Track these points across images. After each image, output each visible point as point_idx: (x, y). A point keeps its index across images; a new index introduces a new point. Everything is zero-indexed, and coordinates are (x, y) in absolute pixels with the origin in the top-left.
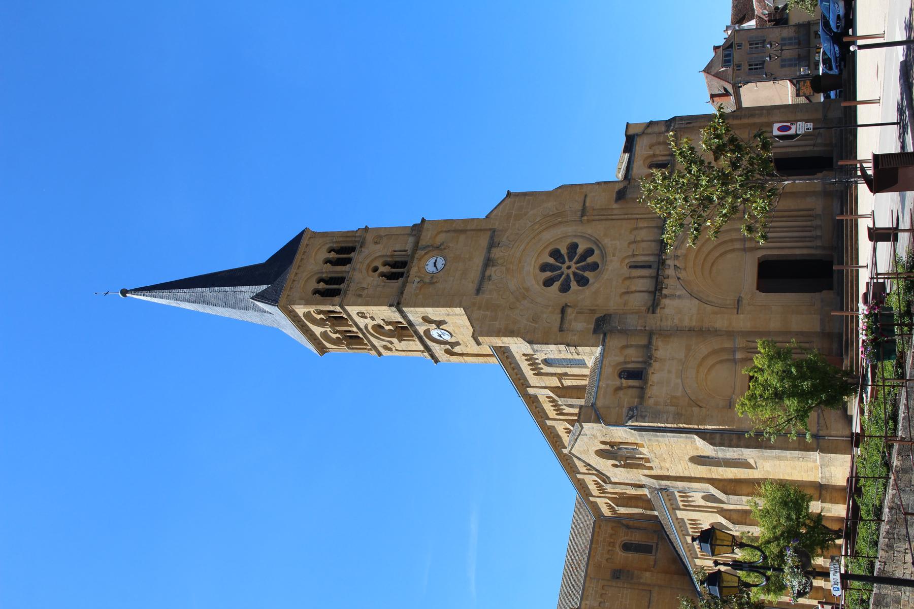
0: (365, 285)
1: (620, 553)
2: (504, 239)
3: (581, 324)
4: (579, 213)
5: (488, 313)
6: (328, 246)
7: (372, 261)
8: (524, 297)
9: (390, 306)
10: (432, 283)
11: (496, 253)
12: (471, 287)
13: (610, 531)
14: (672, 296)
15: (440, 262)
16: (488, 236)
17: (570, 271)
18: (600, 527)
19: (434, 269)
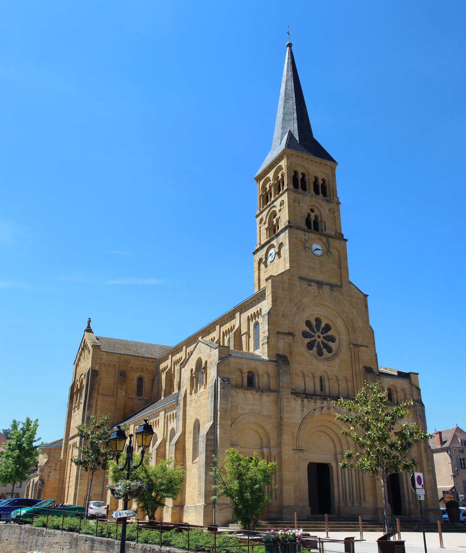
0: (301, 204)
1: (136, 376)
2: (336, 294)
3: (282, 345)
4: (355, 343)
5: (287, 285)
6: (326, 179)
7: (318, 208)
8: (298, 308)
9: (289, 222)
10: (305, 248)
11: (326, 289)
12: (304, 273)
13: (150, 368)
14: (303, 406)
15: (319, 253)
16: (337, 282)
17: (316, 338)
18: (152, 362)
19: (314, 249)
